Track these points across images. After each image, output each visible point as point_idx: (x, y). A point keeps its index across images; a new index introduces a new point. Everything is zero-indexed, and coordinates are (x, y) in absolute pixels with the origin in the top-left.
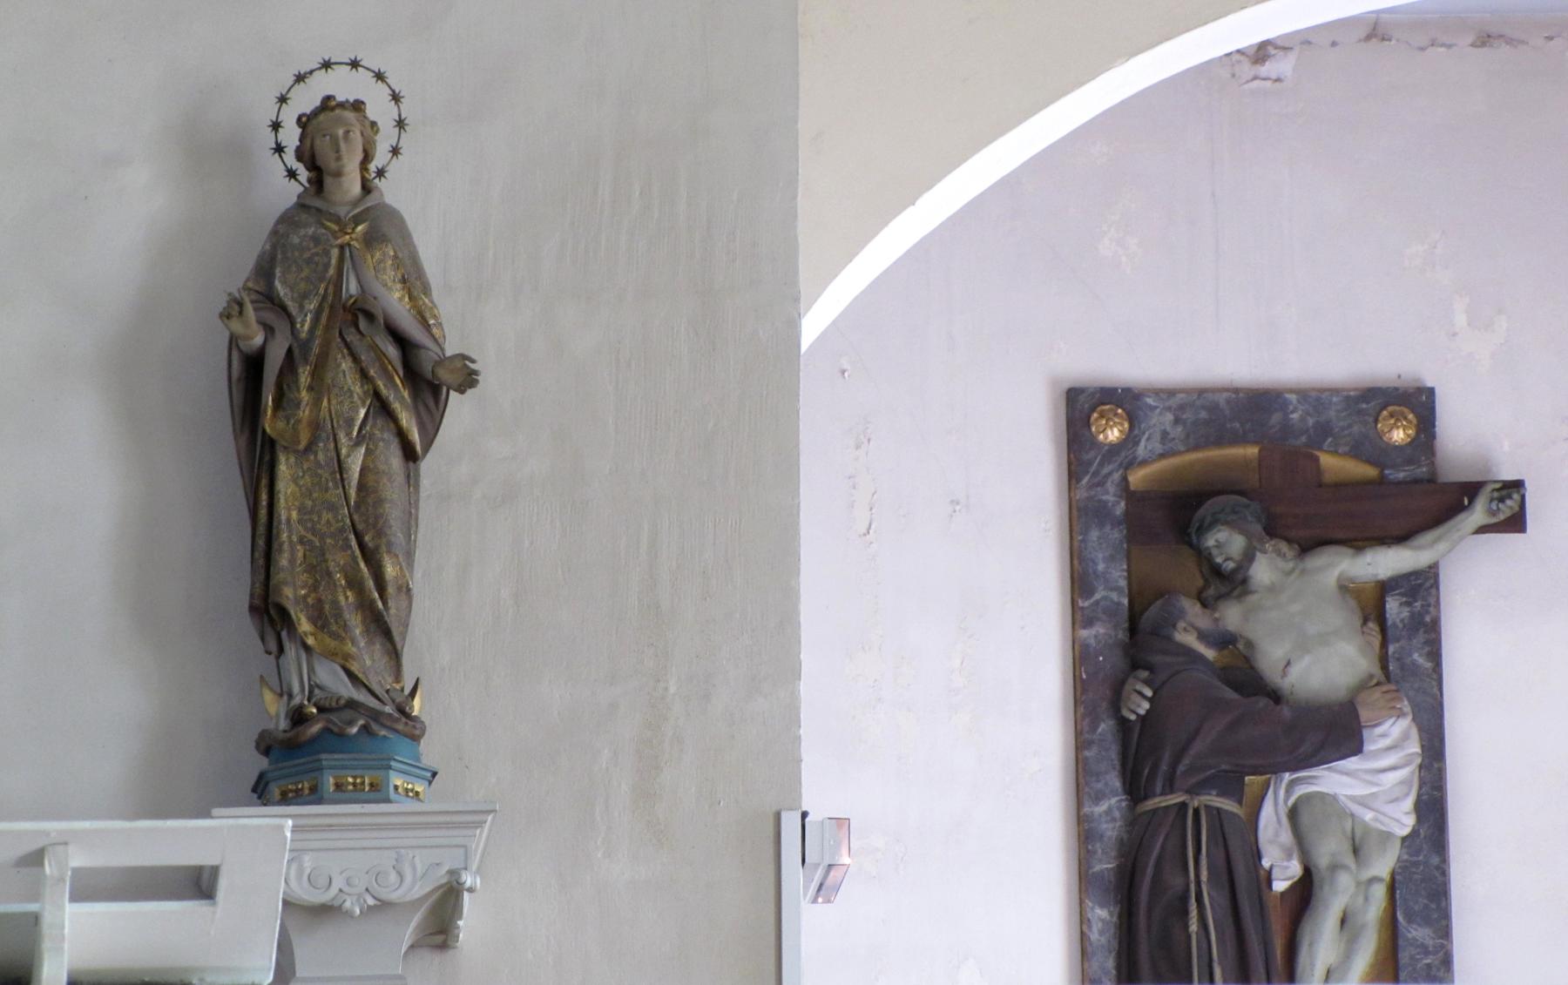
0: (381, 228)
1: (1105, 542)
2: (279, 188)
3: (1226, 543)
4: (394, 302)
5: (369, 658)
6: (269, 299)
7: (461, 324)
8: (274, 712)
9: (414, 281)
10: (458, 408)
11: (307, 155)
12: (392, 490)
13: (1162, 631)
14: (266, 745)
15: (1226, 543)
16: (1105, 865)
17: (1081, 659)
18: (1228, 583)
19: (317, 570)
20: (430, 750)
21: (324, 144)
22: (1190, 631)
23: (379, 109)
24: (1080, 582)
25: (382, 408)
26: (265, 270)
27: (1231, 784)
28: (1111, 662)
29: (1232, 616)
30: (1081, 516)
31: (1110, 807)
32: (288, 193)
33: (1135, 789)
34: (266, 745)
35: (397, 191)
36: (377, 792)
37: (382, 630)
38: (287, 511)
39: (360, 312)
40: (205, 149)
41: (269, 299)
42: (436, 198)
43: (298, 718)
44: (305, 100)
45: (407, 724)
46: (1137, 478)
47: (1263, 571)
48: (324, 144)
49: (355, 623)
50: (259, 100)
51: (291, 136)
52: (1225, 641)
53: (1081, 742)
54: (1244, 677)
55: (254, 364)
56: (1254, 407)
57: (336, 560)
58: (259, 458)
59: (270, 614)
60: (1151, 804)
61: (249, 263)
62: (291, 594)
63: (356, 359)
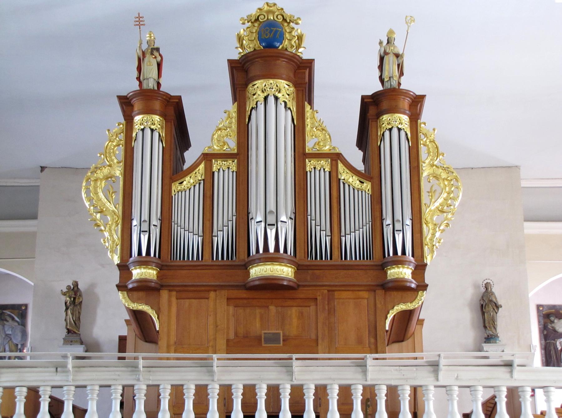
0: (493, 294)
1: (541, 318)
2: (483, 290)
3: (552, 318)
4: (494, 300)
5: (494, 331)
6: (483, 300)
7: (500, 302)
8: (486, 336)
9: (496, 298)
10: (500, 309)
11: (485, 287)
12: (495, 316)
13: (547, 325)
14: (485, 338)
15: (552, 318)
16: (543, 347)
17: (540, 329)
18: (552, 322)
19: (489, 323)
20: (500, 339)
21: (487, 286)
22: (550, 326)
23: (492, 283)
24: (539, 322)
25: (494, 309)
26: (482, 297)
27: (554, 340)
28: (542, 329)
29: (553, 325)
30: (539, 316)
31: (543, 342)
32: (484, 290)
33: (546, 340)
34: (485, 338)
35: (493, 290)
36: (496, 343)
37: (495, 328)
38: (486, 318)
39: (491, 301)
40: (476, 286)
41: (483, 300)
42: (496, 290)
43: (488, 336)
44: (485, 282)
45: (498, 337)
46: (544, 313)
47: (556, 321)
48: (487, 286)
49: (493, 328)
50: (482, 284)
51: (484, 285)
52: (553, 327)
53: (540, 336)
54: (555, 331)
55: (482, 305)
56: (554, 307)
57: (491, 322)
58: (483, 314)
59: (485, 327)
60: (548, 341)
61: (481, 296)
62: (487, 325)
63: (245, 299)
